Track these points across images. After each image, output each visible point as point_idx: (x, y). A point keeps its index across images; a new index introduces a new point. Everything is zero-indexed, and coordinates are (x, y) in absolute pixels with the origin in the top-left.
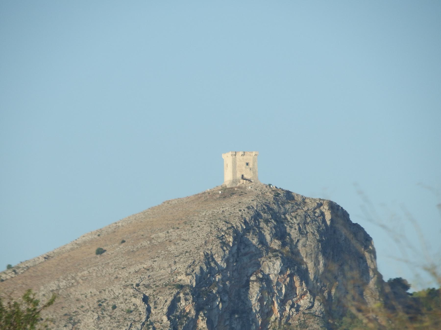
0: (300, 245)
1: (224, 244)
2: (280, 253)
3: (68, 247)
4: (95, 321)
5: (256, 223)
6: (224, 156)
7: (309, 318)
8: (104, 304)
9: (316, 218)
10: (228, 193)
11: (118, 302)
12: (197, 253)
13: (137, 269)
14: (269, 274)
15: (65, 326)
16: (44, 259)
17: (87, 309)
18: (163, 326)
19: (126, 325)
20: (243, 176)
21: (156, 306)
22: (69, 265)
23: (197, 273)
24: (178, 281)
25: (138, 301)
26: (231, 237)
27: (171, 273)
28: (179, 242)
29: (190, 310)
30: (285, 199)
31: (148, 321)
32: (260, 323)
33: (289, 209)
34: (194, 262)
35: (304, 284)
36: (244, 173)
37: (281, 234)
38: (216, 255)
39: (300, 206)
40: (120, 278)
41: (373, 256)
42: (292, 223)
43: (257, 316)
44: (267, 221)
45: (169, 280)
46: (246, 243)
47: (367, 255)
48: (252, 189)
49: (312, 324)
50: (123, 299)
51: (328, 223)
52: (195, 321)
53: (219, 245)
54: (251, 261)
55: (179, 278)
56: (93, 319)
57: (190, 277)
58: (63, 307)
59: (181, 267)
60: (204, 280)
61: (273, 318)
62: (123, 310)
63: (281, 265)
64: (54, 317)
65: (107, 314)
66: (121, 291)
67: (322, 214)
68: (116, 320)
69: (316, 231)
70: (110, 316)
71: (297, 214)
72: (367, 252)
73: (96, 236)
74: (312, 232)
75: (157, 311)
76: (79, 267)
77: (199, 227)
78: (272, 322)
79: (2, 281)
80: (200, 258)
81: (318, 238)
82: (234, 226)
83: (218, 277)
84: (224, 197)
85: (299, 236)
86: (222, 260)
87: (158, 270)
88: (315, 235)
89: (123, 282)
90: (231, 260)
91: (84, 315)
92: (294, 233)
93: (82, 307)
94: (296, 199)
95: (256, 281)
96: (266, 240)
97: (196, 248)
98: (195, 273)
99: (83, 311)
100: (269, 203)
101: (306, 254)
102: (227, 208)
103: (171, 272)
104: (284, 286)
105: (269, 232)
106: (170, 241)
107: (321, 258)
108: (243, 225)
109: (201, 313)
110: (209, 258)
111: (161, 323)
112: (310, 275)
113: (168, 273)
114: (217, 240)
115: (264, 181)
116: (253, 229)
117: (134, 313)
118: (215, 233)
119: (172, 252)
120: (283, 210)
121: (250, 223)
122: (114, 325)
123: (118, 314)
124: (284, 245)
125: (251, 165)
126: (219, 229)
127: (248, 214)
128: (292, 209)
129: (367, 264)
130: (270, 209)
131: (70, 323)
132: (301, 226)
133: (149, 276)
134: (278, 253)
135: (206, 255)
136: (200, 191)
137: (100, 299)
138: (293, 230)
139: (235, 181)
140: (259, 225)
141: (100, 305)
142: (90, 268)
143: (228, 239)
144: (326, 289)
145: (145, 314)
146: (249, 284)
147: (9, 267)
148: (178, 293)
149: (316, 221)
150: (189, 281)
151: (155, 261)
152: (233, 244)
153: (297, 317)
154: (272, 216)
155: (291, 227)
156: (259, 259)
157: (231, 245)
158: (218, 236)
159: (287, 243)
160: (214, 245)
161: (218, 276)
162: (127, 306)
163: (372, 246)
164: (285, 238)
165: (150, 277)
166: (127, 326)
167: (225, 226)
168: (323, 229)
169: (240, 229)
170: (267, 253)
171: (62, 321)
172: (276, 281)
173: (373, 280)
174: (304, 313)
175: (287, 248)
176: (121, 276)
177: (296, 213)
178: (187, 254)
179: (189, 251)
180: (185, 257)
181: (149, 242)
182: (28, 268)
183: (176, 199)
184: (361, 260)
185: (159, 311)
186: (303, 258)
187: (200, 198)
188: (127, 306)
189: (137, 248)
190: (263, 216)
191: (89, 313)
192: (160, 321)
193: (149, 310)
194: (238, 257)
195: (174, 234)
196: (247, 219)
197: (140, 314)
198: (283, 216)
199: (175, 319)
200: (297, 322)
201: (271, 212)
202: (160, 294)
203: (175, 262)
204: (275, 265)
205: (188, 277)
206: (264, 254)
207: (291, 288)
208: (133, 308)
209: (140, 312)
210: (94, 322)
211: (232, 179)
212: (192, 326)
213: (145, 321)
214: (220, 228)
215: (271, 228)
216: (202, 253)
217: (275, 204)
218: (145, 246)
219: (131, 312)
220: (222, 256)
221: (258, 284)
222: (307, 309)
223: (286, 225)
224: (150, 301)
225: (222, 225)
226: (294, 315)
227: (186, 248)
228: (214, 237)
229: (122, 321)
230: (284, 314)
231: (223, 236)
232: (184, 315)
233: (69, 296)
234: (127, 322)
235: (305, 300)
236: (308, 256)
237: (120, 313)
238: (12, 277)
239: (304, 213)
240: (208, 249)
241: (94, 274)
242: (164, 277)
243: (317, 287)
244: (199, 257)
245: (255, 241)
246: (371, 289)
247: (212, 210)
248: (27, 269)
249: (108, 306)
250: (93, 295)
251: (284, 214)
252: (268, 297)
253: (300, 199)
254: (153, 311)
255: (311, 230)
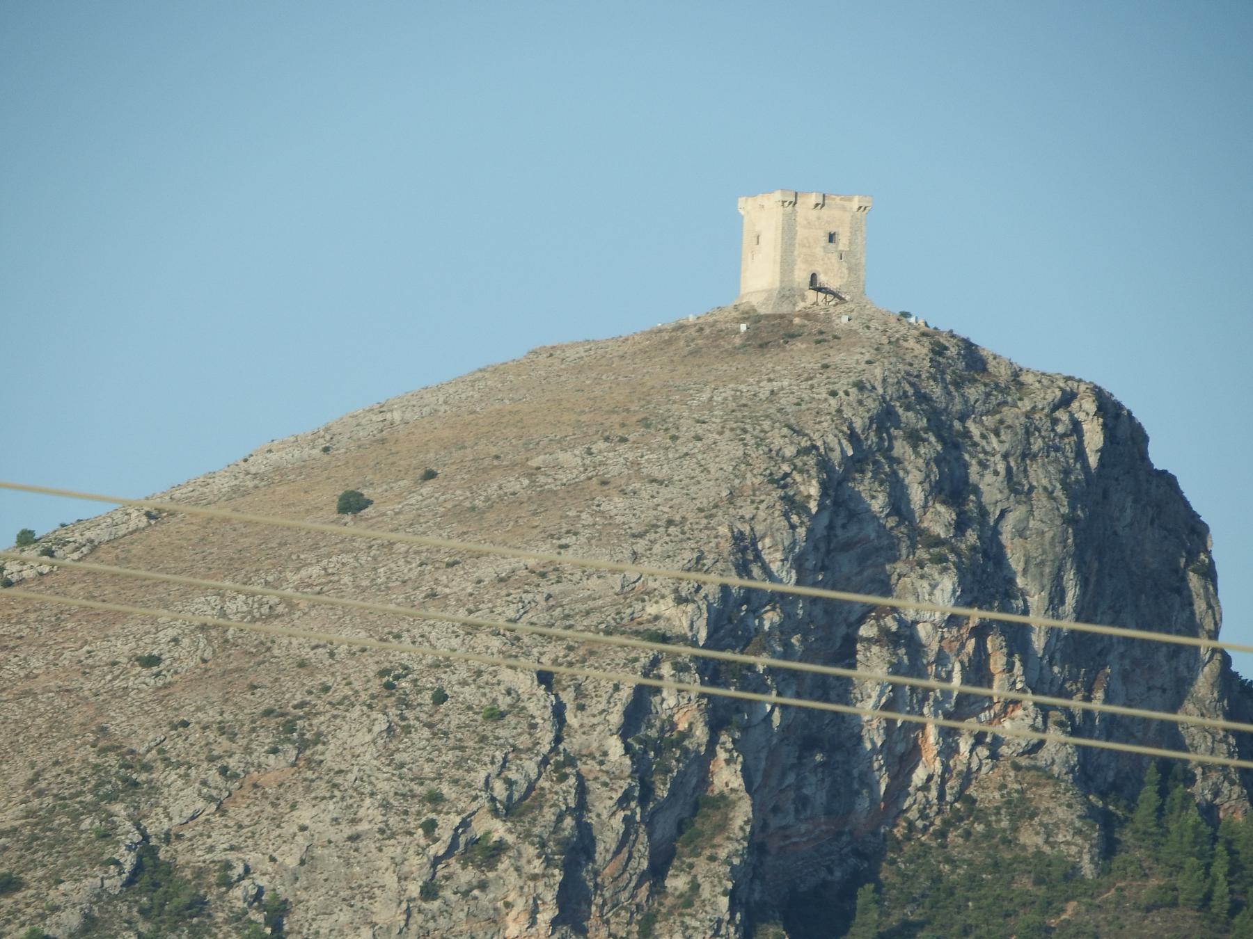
0: (1007, 527)
1: (793, 504)
2: (954, 550)
3: (223, 484)
4: (380, 742)
5: (881, 439)
6: (746, 206)
7: (1038, 785)
8: (404, 684)
9: (1057, 440)
10: (770, 332)
11: (449, 680)
12: (706, 528)
13: (504, 568)
14: (915, 623)
15: (274, 751)
16: (145, 519)
17: (346, 697)
18: (607, 772)
19: (487, 760)
20: (814, 276)
21: (583, 701)
22: (245, 542)
23: (710, 597)
24: (649, 621)
25: (524, 683)
26: (814, 482)
27: (623, 593)
28: (638, 485)
29: (691, 725)
30: (961, 365)
31: (558, 754)
32: (883, 788)
33: (977, 401)
34: (699, 559)
35: (1018, 664)
36: (817, 268)
37: (953, 488)
38: (768, 541)
39: (1008, 394)
40: (446, 596)
41: (1211, 588)
42: (986, 453)
43: (876, 765)
44: (914, 439)
45: (618, 613)
46: (852, 505)
47: (1194, 581)
48: (855, 325)
49: (1052, 805)
50: (469, 670)
51: (1093, 460)
52: (702, 763)
53: (778, 506)
54: (860, 573)
55: (652, 609)
56: (370, 731)
57: (690, 608)
58: (253, 687)
59: (659, 572)
60: (730, 620)
61: (919, 776)
62: (470, 708)
63: (954, 591)
64: (228, 716)
65: (417, 719)
66: (459, 641)
67: (1076, 427)
68: (451, 742)
69: (1058, 486)
70: (430, 726)
71: (1001, 422)
72: (1193, 571)
73: (317, 452)
74: (1045, 489)
75: (586, 721)
76: (283, 552)
77: (698, 438)
78: (919, 789)
79: (8, 584)
80: (718, 544)
81: (1065, 510)
82: (819, 443)
83: (771, 618)
84: (761, 346)
85: (1008, 499)
86: (786, 559)
87: (577, 577)
88: (1054, 499)
89: (462, 614)
90: (811, 563)
91: (335, 717)
92: (991, 487)
93: (326, 689)
94: (991, 370)
95: (875, 641)
96: (909, 502)
97: (701, 510)
98: (706, 597)
99: (330, 703)
100: (918, 376)
101: (1026, 562)
102: (786, 383)
103: (623, 587)
104: (957, 667)
105: (920, 476)
106: (604, 483)
107: (1070, 580)
108: (845, 442)
109: (724, 738)
110: (746, 548)
111: (601, 763)
112: (1034, 637)
113: (611, 592)
114: (770, 487)
115: (885, 299)
116: (875, 462)
117: (511, 719)
118: (761, 464)
119: (619, 519)
120: (958, 406)
121: (866, 439)
122: (444, 758)
123: (455, 720)
124: (961, 526)
125: (843, 242)
126: (771, 450)
127: (861, 409)
128: (985, 403)
129: (1193, 613)
130: (924, 398)
131: (289, 740)
132: (1012, 464)
133: (549, 596)
134: (944, 550)
135: (738, 538)
136: (664, 320)
137: (387, 665)
138: (989, 477)
139: (787, 293)
140: (891, 448)
141: (389, 686)
142: (329, 556)
143: (802, 488)
144: (1078, 690)
145: (548, 725)
146: (855, 652)
147: (26, 538)
148: (655, 662)
149: (1057, 449)
150: (686, 624)
151: (566, 546)
152: (819, 505)
153: (996, 776)
154: (928, 420)
155: (983, 465)
156: (888, 567)
157: (814, 510)
158: (771, 474)
159: (970, 519)
160: (763, 506)
161: (770, 614)
162: (484, 695)
163: (1208, 553)
164: (965, 501)
165: (552, 602)
166: (493, 763)
167: (792, 443)
168: (1077, 481)
169: (836, 457)
170: (913, 547)
171: (262, 732)
172: (935, 647)
173: (1207, 669)
174: (1017, 767)
175: (972, 537)
176: (447, 591)
177: (998, 417)
178: (672, 529)
179: (677, 518)
180: (667, 539)
181: (526, 482)
182: (94, 547)
183: (577, 344)
184: (1177, 599)
185: (595, 721)
186: (1015, 573)
187: (669, 342)
188: (484, 695)
189: (487, 499)
190: (903, 419)
191: (356, 712)
192: (597, 755)
193: (559, 712)
194: (828, 552)
195: (615, 461)
196: (858, 424)
197: (533, 726)
198: (957, 425)
199: (645, 752)
200: (997, 795)
201: (925, 407)
202: (592, 660)
203: (635, 556)
204: (937, 592)
205: (682, 607)
206: (904, 552)
207: (978, 671)
208: (504, 703)
209: (533, 717)
210: (374, 742)
211: (777, 285)
212: (694, 781)
213: (550, 752)
214: (775, 447)
215: (927, 464)
216: (724, 530)
217: (935, 379)
218: (514, 494)
219: (502, 715)
220: (787, 543)
221: (885, 653)
222: (1023, 754)
223: (967, 457)
224: (559, 682)
225: (778, 439)
226: (984, 770)
227: (666, 509)
228: (760, 478)
229: (471, 743)
230: (951, 763)
231: (786, 475)
232: (672, 740)
233: (269, 649)
234: (489, 751)
235: (1018, 722)
236: (1032, 569)
237: (463, 718)
238: (41, 574)
239: (1023, 420)
240: (742, 517)
241: (346, 579)
242: (600, 602)
243: (1052, 680)
244: (714, 541)
245: (878, 504)
246: (1202, 701)
247: (732, 385)
248: (93, 550)
249: (419, 692)
250: (355, 648)
251: (963, 418)
252: (911, 700)
253: (1004, 374)
254: (572, 719)
255: (1045, 482)
